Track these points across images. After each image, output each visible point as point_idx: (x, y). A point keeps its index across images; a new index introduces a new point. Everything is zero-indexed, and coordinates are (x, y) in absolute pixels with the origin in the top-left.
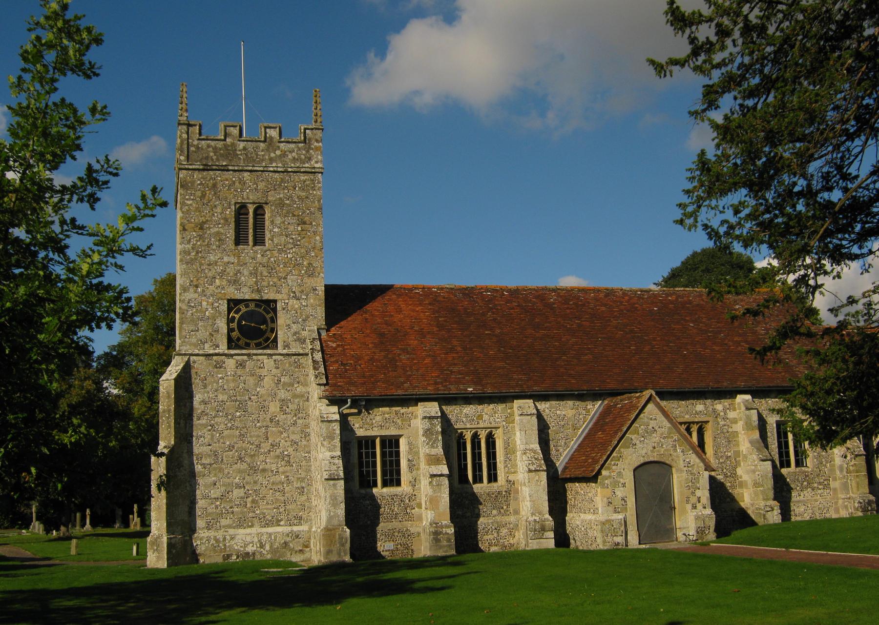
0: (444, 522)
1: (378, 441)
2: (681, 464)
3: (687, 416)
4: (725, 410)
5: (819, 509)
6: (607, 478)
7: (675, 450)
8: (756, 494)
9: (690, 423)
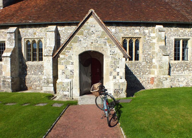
0: (8, 77)
2: (109, 53)
3: (130, 35)
4: (149, 33)
6: (62, 59)
8: (160, 72)
9: (132, 38)
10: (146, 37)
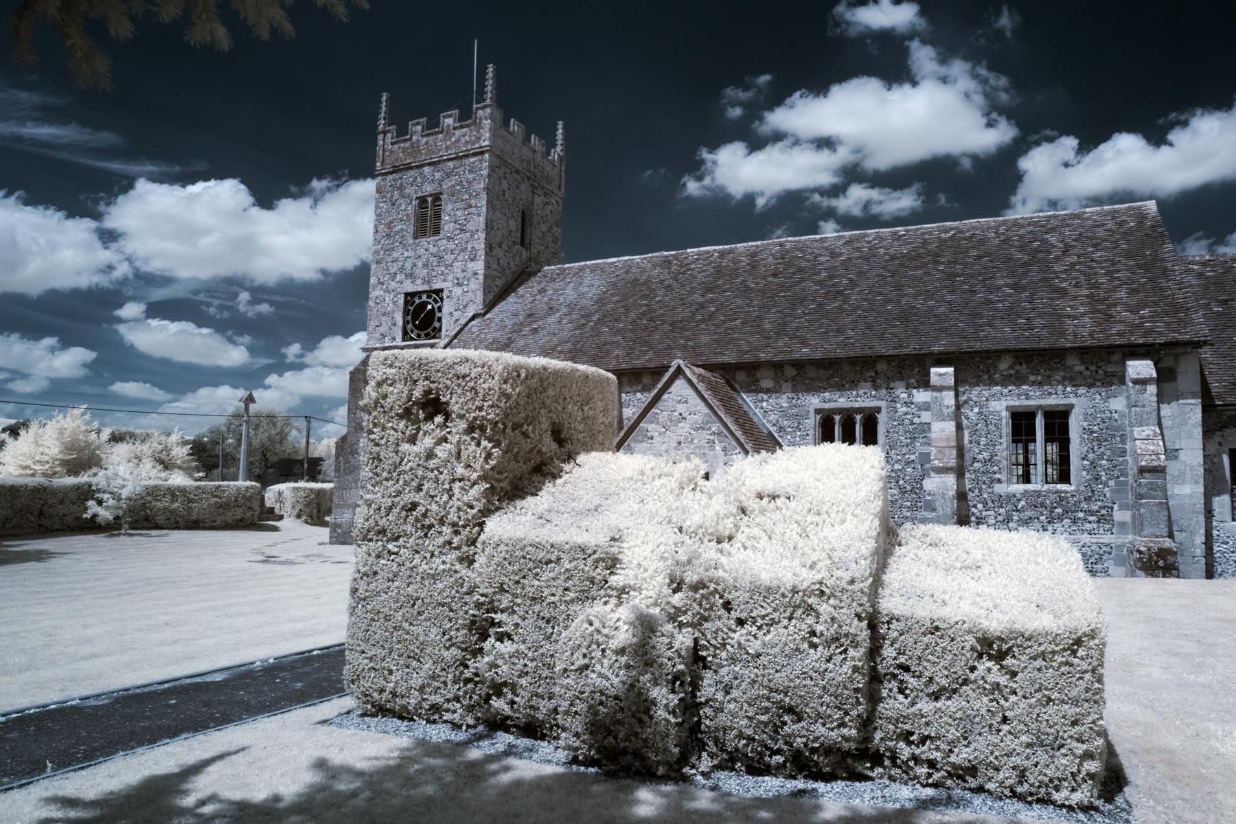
1: (1040, 422)
3: (841, 400)
7: (712, 447)
10: (899, 405)
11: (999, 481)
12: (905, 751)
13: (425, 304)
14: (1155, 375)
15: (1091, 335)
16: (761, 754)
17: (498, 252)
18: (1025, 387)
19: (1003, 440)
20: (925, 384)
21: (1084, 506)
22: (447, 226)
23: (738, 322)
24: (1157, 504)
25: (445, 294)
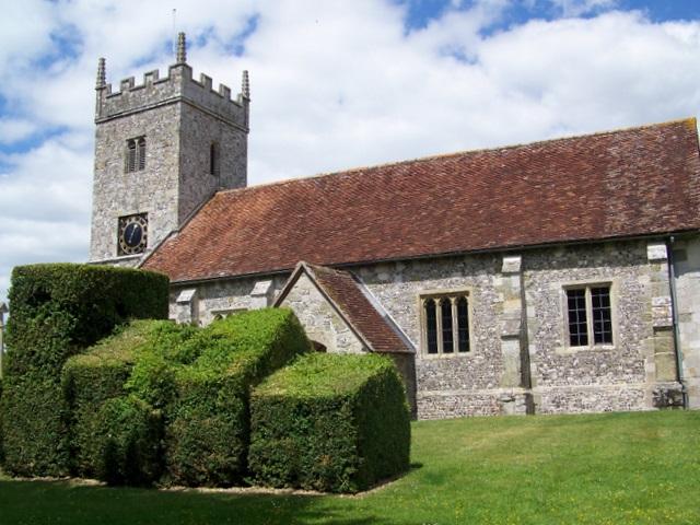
1: (588, 297)
3: (440, 287)
5: (620, 400)
7: (328, 328)
11: (559, 345)
12: (265, 469)
13: (132, 225)
14: (666, 256)
15: (623, 227)
16: (194, 475)
17: (190, 180)
18: (575, 270)
19: (561, 313)
20: (498, 270)
21: (622, 361)
22: (149, 164)
23: (366, 229)
24: (666, 356)
25: (149, 217)
